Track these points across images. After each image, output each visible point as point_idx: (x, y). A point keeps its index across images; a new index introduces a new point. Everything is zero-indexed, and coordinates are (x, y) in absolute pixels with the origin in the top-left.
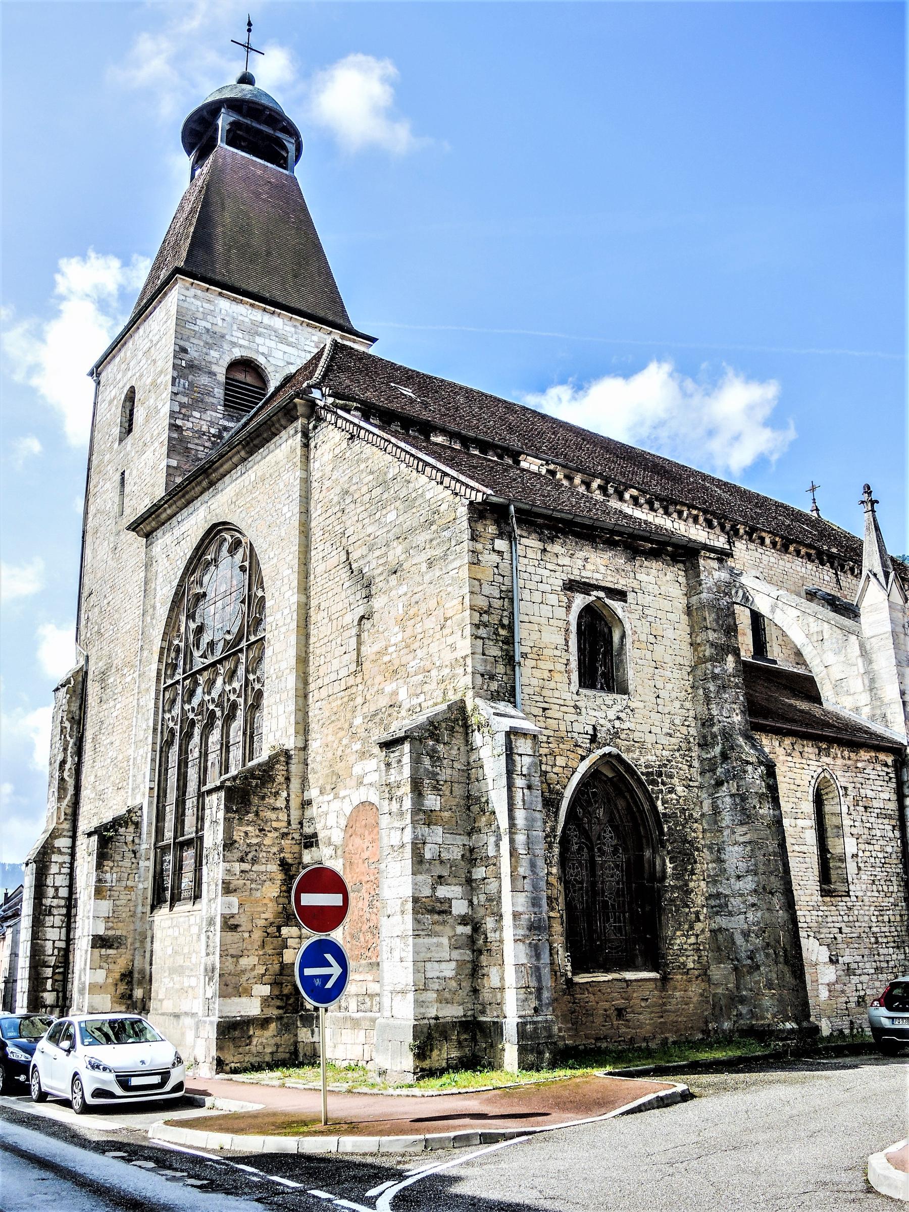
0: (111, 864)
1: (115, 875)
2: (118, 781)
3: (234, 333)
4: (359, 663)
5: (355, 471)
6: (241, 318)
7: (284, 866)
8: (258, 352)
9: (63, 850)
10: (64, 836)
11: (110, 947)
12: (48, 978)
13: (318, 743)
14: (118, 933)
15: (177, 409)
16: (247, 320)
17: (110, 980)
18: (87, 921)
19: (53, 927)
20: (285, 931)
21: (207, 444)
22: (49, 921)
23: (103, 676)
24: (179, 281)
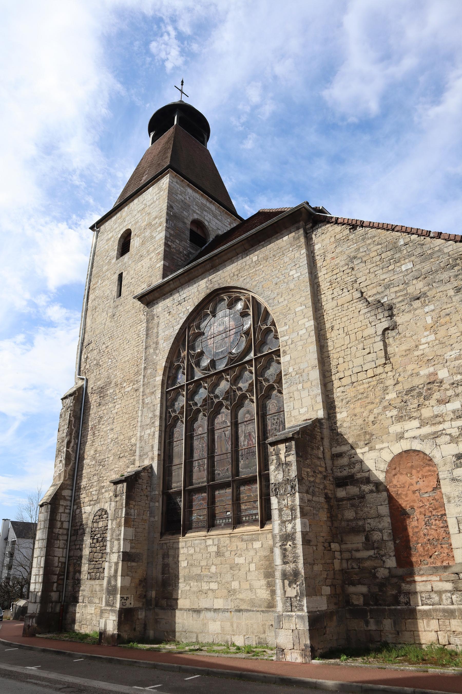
0: (134, 503)
1: (136, 510)
2: (119, 453)
3: (194, 206)
4: (387, 357)
5: (361, 245)
6: (197, 200)
7: (327, 497)
8: (204, 219)
9: (67, 498)
10: (68, 489)
11: (133, 561)
12: (55, 582)
13: (344, 414)
14: (138, 551)
15: (168, 236)
16: (199, 202)
17: (133, 585)
18: (116, 543)
19: (59, 548)
20: (333, 546)
21: (182, 258)
22: (57, 544)
23: (102, 391)
24: (170, 172)
